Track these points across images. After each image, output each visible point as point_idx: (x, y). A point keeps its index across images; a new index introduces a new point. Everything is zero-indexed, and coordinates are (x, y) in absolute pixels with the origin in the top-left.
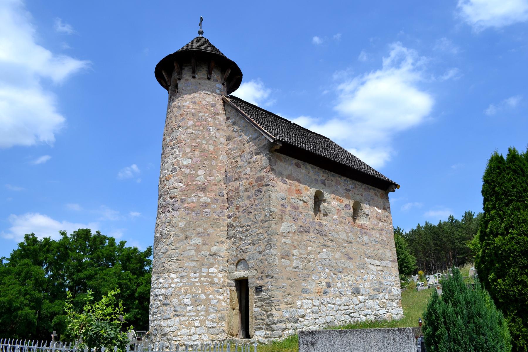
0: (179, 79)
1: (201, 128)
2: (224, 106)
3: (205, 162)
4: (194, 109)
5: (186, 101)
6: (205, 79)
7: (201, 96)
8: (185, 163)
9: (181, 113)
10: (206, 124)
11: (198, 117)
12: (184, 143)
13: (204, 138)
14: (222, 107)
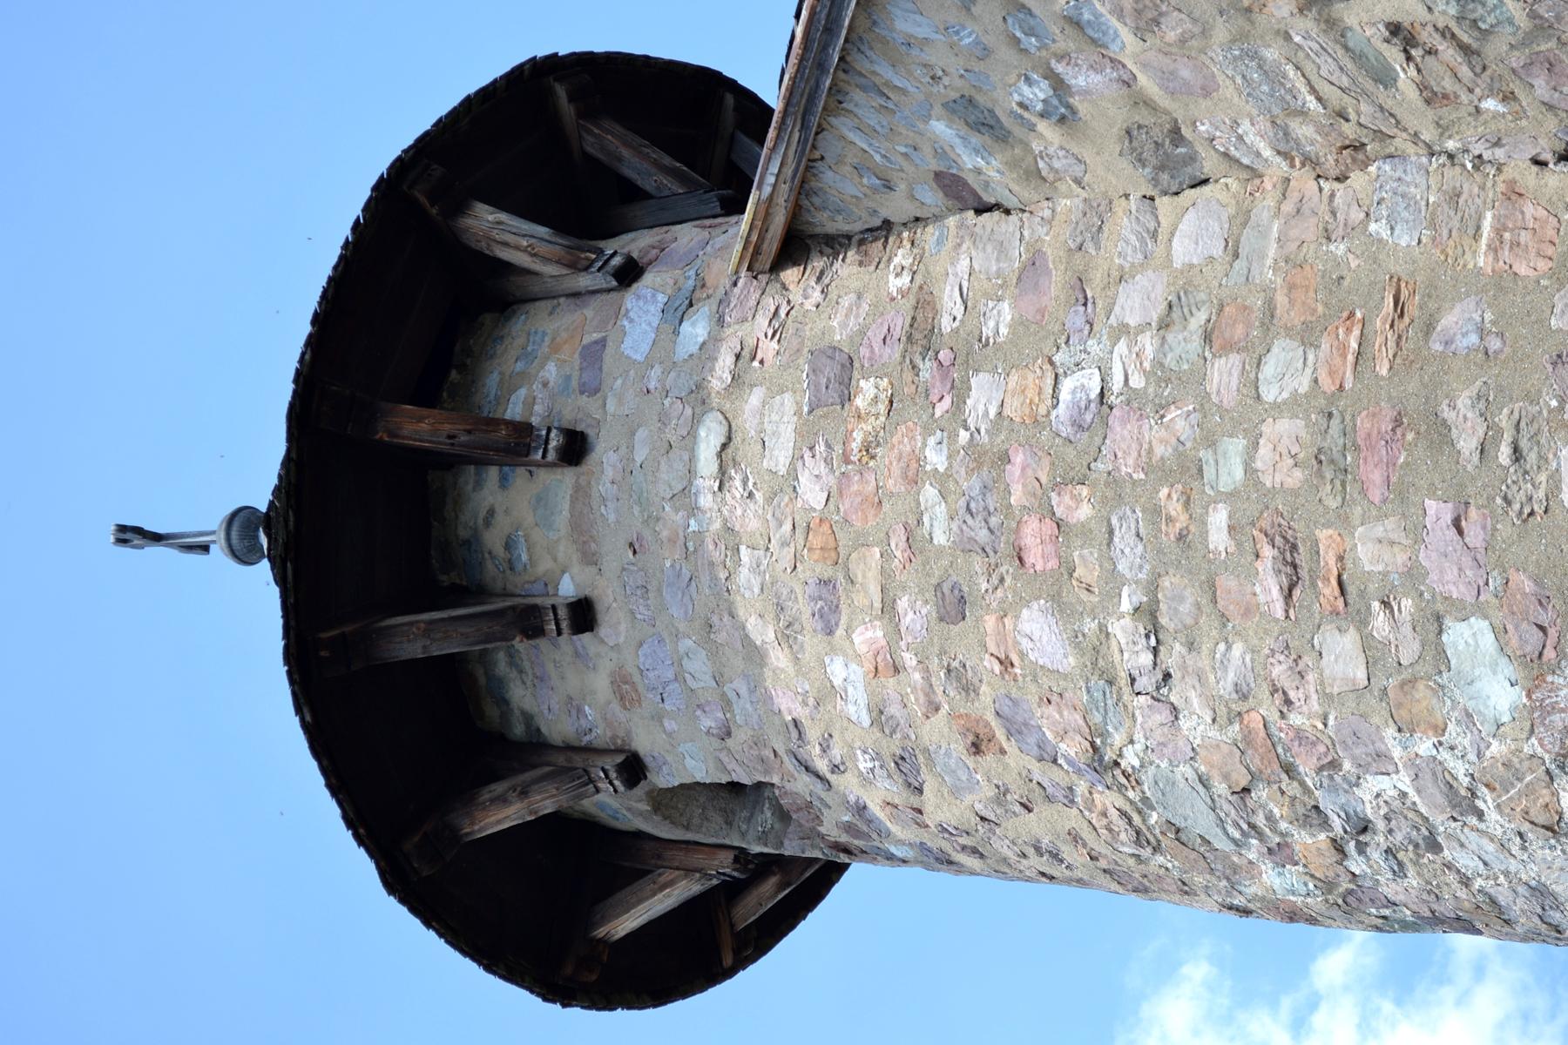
0: (633, 769)
1: (1080, 509)
2: (835, 244)
3: (1467, 444)
4: (888, 609)
5: (827, 694)
6: (581, 493)
7: (749, 519)
8: (1499, 694)
9: (959, 747)
10: (1029, 445)
11: (966, 546)
12: (1268, 709)
13: (1186, 470)
14: (847, 269)
